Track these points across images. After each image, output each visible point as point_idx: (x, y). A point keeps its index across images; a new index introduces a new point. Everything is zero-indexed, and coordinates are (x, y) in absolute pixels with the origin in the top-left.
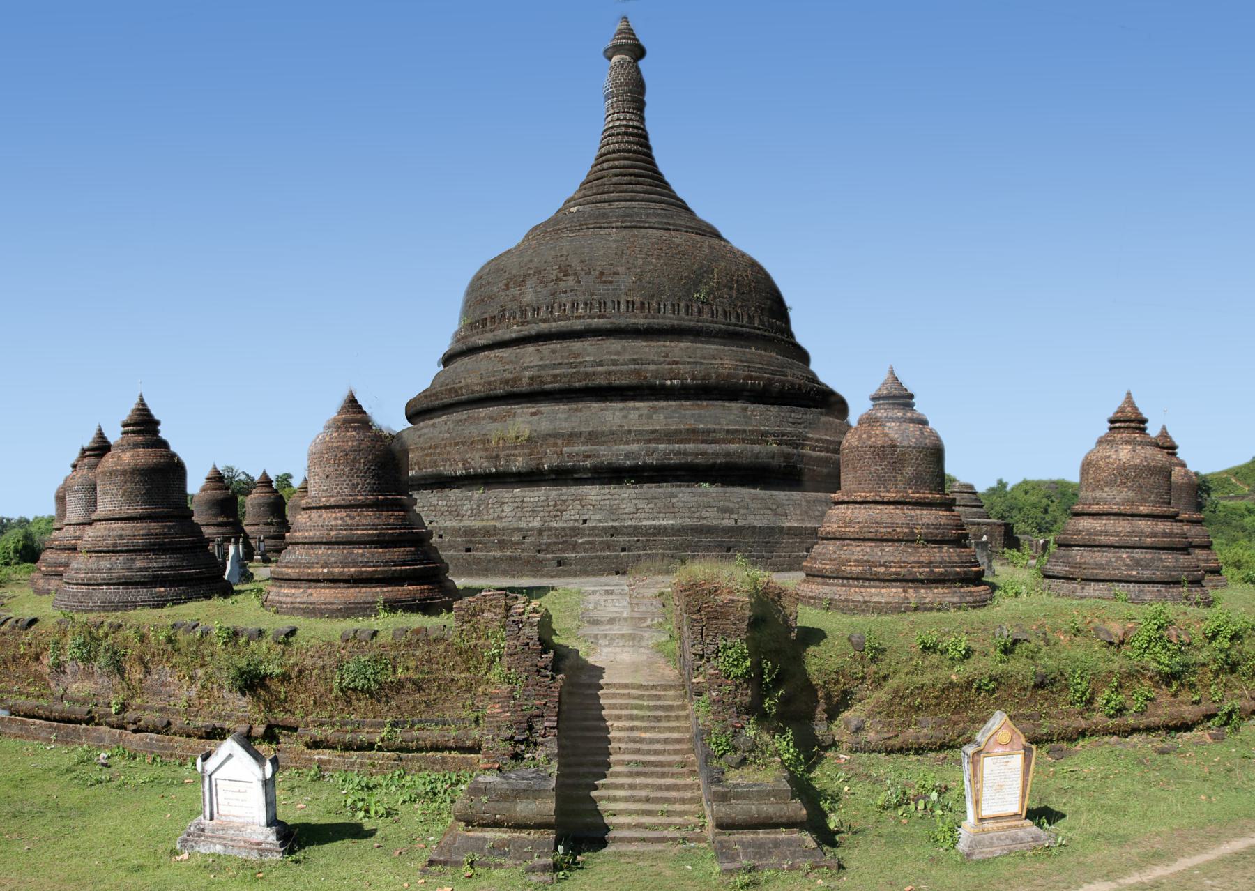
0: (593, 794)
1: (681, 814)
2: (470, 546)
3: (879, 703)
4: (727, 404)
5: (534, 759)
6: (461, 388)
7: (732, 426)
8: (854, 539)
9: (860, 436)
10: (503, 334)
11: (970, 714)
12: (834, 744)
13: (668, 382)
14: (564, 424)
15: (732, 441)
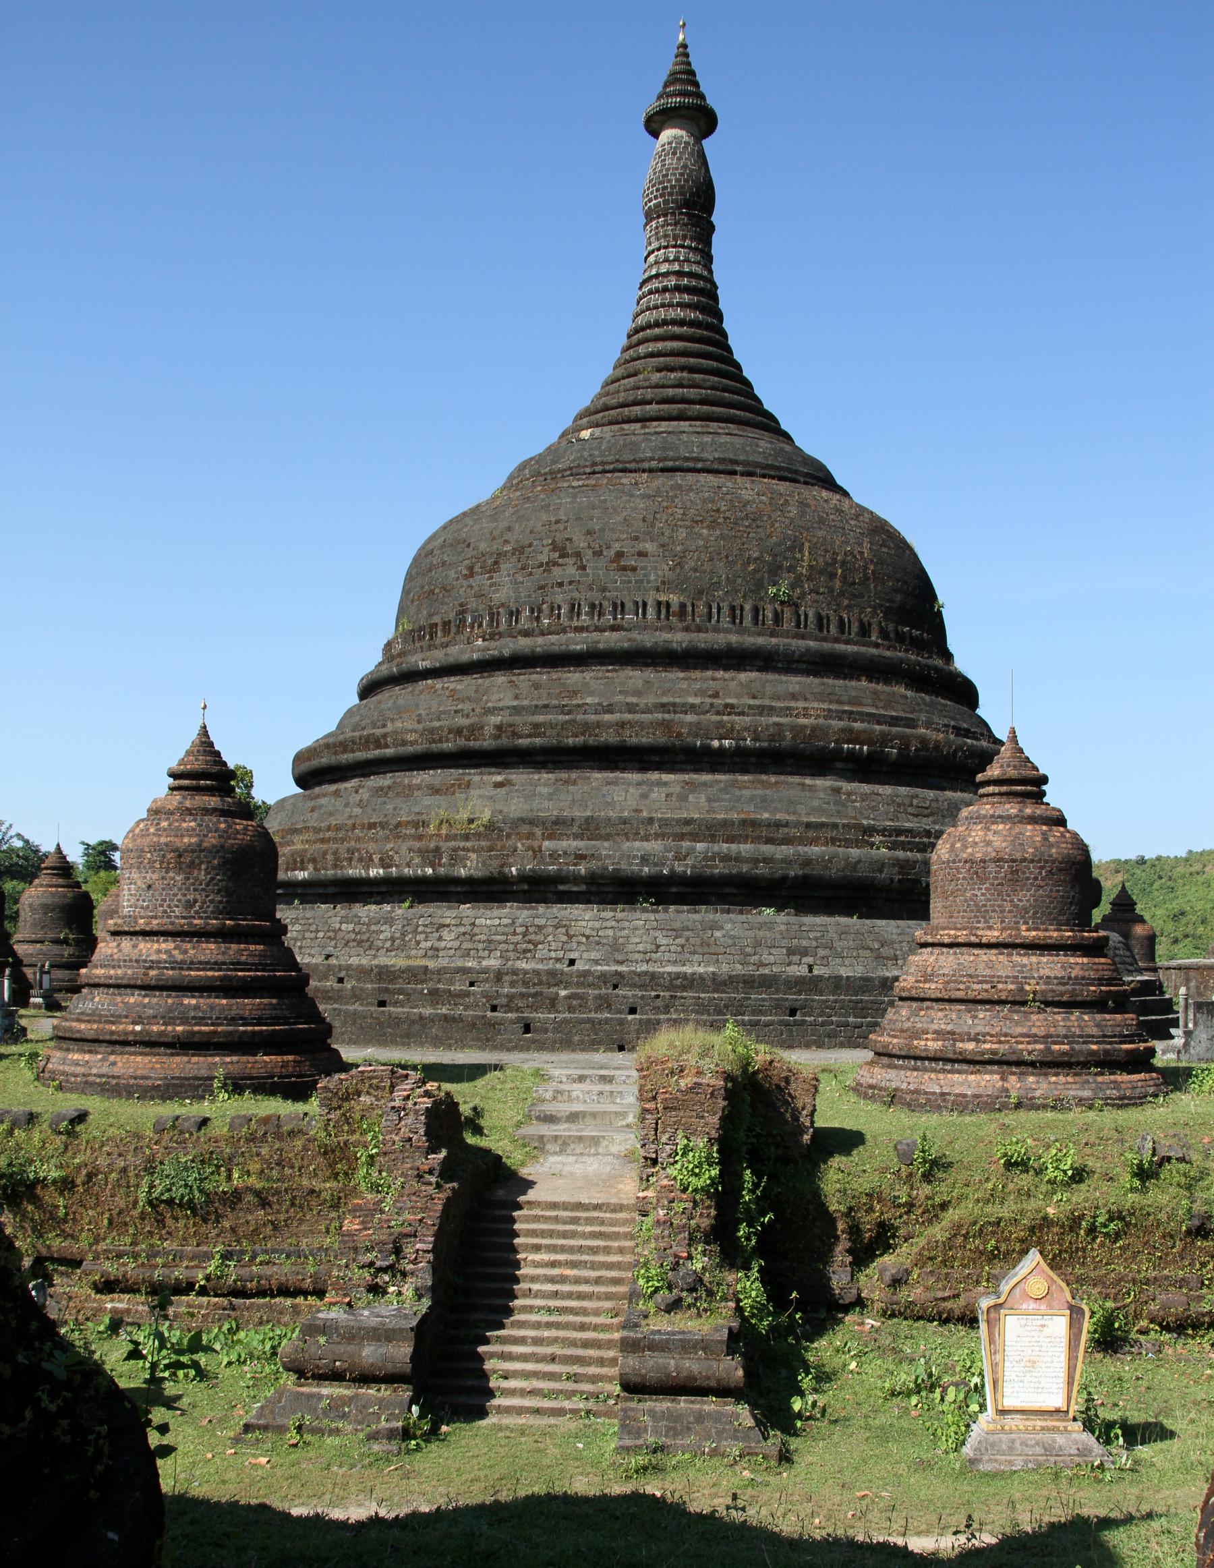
0: (481, 1349)
1: (594, 1379)
2: (386, 997)
3: (932, 1245)
4: (808, 781)
5: (400, 1293)
6: (385, 736)
7: (813, 814)
8: (937, 1000)
9: (953, 846)
10: (459, 652)
11: (1079, 1270)
12: (860, 1303)
13: (716, 743)
15: (814, 841)
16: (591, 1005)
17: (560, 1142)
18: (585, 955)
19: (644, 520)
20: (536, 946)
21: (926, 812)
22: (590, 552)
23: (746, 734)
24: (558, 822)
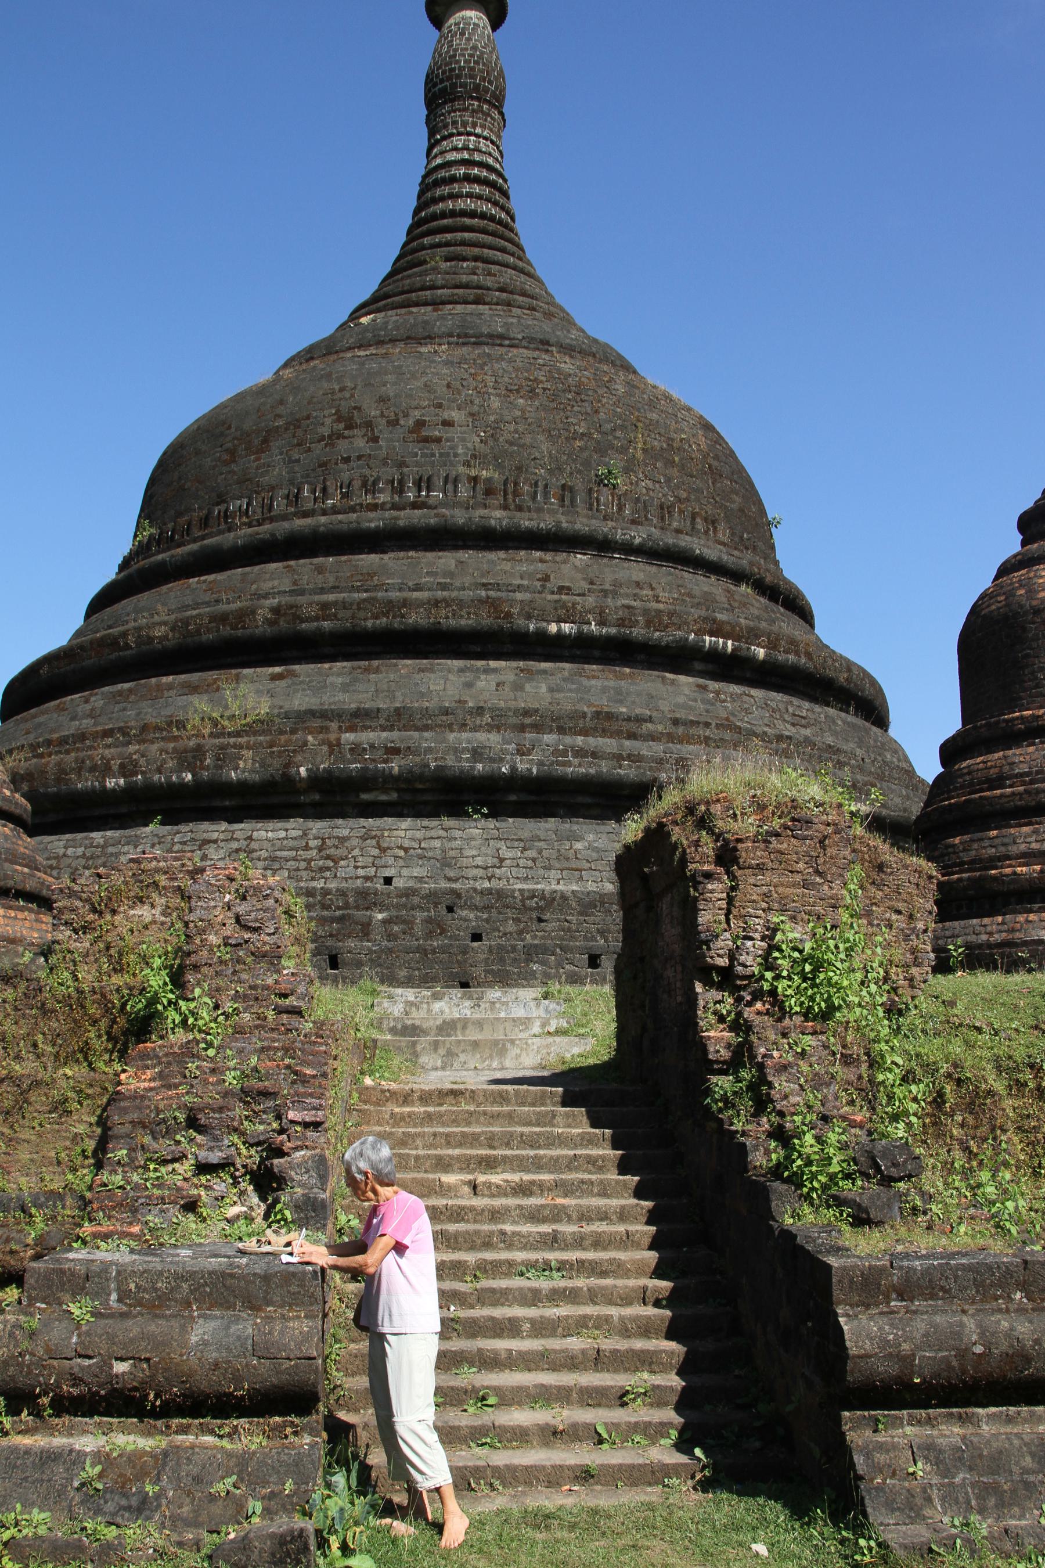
6: (124, 634)
14: (340, 697)
16: (418, 930)
17: (442, 1051)
18: (405, 872)
19: (448, 386)
20: (336, 862)
21: (803, 722)
22: (384, 421)
23: (591, 617)
24: (357, 714)
